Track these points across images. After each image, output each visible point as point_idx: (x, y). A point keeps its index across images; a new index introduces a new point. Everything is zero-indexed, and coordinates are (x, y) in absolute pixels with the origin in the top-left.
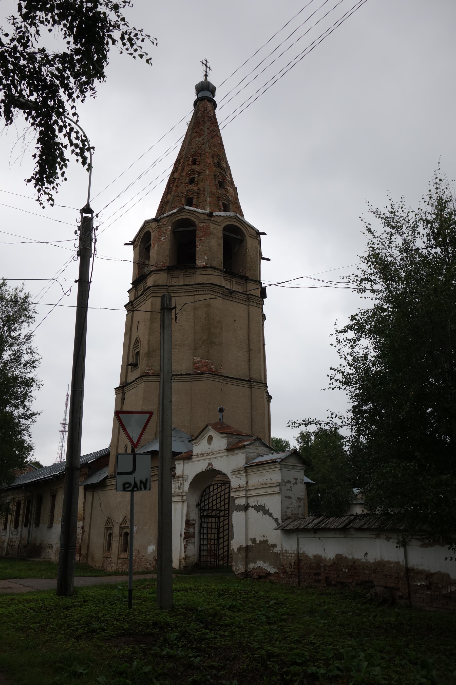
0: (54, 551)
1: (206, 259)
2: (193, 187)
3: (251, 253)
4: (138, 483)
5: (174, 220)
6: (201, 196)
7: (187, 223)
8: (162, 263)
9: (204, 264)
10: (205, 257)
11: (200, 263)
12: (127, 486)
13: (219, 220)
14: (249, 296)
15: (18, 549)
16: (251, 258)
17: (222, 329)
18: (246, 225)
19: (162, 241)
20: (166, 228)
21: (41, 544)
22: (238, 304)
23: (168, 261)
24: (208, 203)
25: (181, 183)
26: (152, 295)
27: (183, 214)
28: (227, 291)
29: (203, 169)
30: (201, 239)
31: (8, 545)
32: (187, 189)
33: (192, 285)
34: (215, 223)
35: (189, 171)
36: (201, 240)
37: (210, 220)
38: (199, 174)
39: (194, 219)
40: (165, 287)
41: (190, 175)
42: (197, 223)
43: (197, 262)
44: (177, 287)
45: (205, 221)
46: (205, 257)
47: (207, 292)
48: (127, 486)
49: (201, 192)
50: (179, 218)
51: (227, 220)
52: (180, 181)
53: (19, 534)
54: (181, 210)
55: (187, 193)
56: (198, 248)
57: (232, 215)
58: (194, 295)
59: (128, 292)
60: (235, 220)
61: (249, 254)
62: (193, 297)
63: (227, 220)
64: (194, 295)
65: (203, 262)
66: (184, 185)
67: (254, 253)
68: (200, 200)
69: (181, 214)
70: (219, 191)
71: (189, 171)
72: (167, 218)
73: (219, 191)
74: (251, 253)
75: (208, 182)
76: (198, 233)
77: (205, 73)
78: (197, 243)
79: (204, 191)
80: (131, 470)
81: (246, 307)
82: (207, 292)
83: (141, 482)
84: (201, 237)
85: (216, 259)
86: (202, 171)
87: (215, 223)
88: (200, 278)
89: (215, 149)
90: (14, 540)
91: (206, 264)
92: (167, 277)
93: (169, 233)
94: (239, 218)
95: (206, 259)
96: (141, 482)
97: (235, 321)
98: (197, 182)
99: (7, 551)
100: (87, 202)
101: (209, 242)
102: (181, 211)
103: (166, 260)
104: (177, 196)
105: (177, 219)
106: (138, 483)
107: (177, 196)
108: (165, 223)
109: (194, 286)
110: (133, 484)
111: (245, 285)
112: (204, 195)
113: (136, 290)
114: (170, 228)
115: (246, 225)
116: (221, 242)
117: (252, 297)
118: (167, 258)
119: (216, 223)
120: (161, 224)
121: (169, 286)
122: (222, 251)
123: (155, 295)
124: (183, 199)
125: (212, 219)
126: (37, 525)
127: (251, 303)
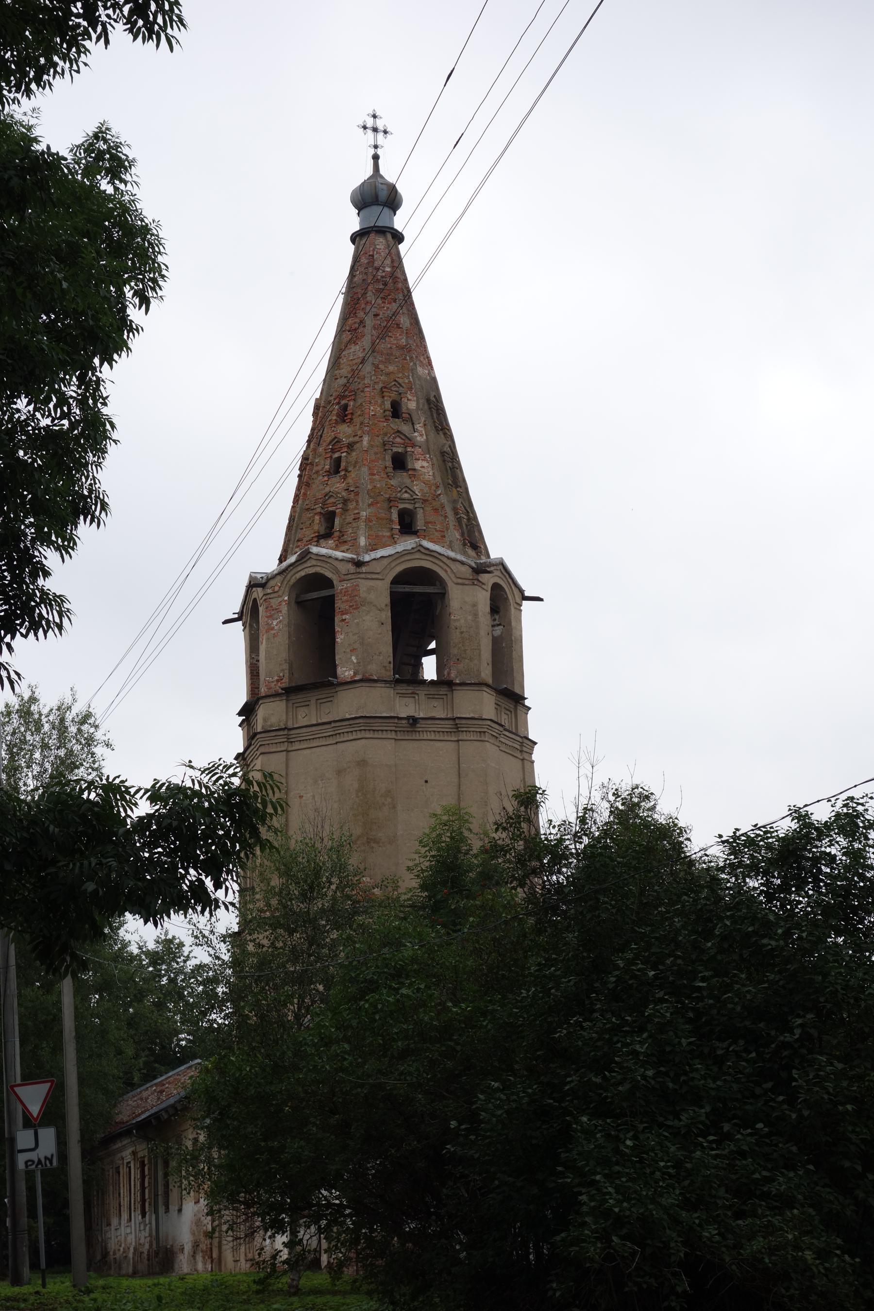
0: (186, 1256)
1: (355, 661)
2: (337, 485)
3: (462, 621)
4: (43, 1160)
5: (293, 581)
6: (351, 506)
7: (319, 582)
8: (276, 678)
9: (352, 673)
10: (353, 658)
11: (345, 672)
12: (29, 1163)
13: (377, 567)
14: (457, 721)
15: (148, 1260)
16: (462, 633)
17: (394, 807)
18: (445, 560)
19: (273, 629)
20: (280, 599)
21: (172, 1246)
22: (432, 743)
23: (287, 671)
24: (362, 525)
25: (317, 472)
26: (262, 750)
27: (308, 564)
28: (404, 722)
29: (359, 433)
30: (344, 617)
31: (134, 1254)
32: (327, 489)
33: (330, 723)
34: (369, 576)
35: (329, 444)
36: (343, 620)
37: (360, 573)
38: (350, 446)
39: (329, 574)
40: (281, 733)
41: (333, 451)
42: (335, 582)
43: (339, 670)
44: (304, 730)
45: (350, 577)
46: (353, 658)
47: (359, 735)
48: (29, 1163)
49: (352, 496)
50: (303, 574)
51: (398, 561)
52: (315, 469)
53: (147, 1228)
54: (305, 556)
55: (324, 503)
56: (339, 638)
57: (409, 547)
58: (337, 743)
59: (240, 726)
60: (417, 556)
61: (457, 624)
62: (335, 746)
63: (398, 561)
64: (337, 743)
65: (350, 670)
66: (321, 477)
67: (470, 618)
68: (350, 518)
69: (306, 565)
70: (393, 482)
71: (329, 444)
72: (279, 578)
73: (393, 482)
74: (462, 621)
75: (365, 469)
76: (338, 604)
77: (372, 151)
78: (337, 629)
79: (357, 494)
80: (33, 1146)
81: (453, 745)
82: (359, 735)
83: (46, 1158)
84: (343, 613)
85: (375, 657)
86: (357, 439)
87: (369, 576)
88: (347, 704)
89: (391, 368)
90: (142, 1241)
91: (355, 674)
92: (287, 707)
93: (284, 609)
94: (428, 549)
95: (355, 661)
96: (46, 1158)
97: (426, 782)
98: (346, 470)
99: (134, 1267)
100: (369, 172)
101: (358, 624)
102: (303, 558)
103: (283, 670)
104: (308, 509)
105: (298, 576)
106: (43, 1160)
107: (308, 509)
108: (277, 589)
109: (333, 725)
110: (36, 1161)
111: (449, 697)
112: (357, 502)
113: (249, 725)
114: (286, 598)
115: (445, 560)
116: (386, 615)
117: (464, 722)
118: (286, 666)
119: (372, 576)
120: (269, 591)
121: (290, 729)
122: (389, 637)
123: (267, 750)
124: (317, 517)
125: (364, 569)
126: (167, 1210)
127: (463, 736)
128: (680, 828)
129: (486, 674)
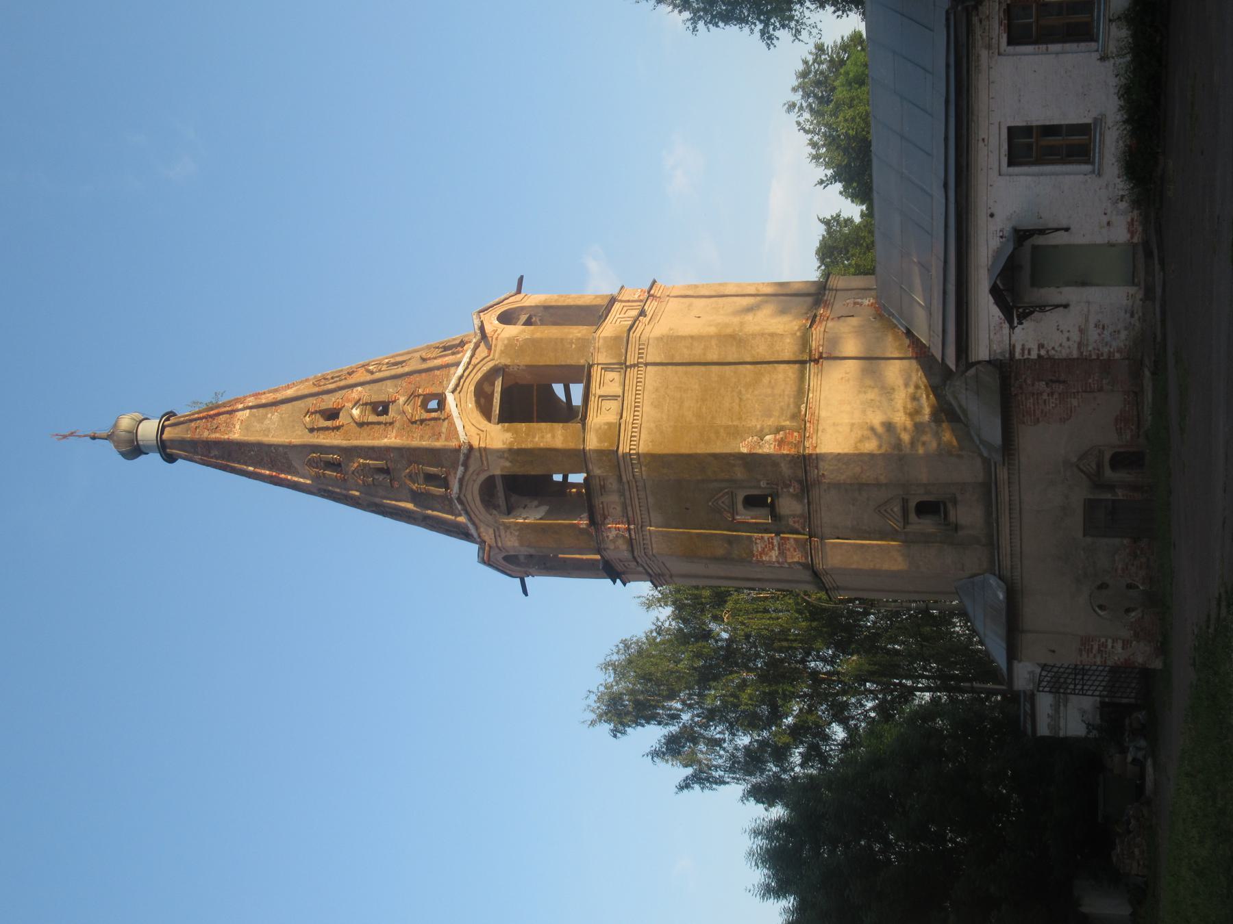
100: (109, 445)
128: (1098, 484)
129: (577, 332)
